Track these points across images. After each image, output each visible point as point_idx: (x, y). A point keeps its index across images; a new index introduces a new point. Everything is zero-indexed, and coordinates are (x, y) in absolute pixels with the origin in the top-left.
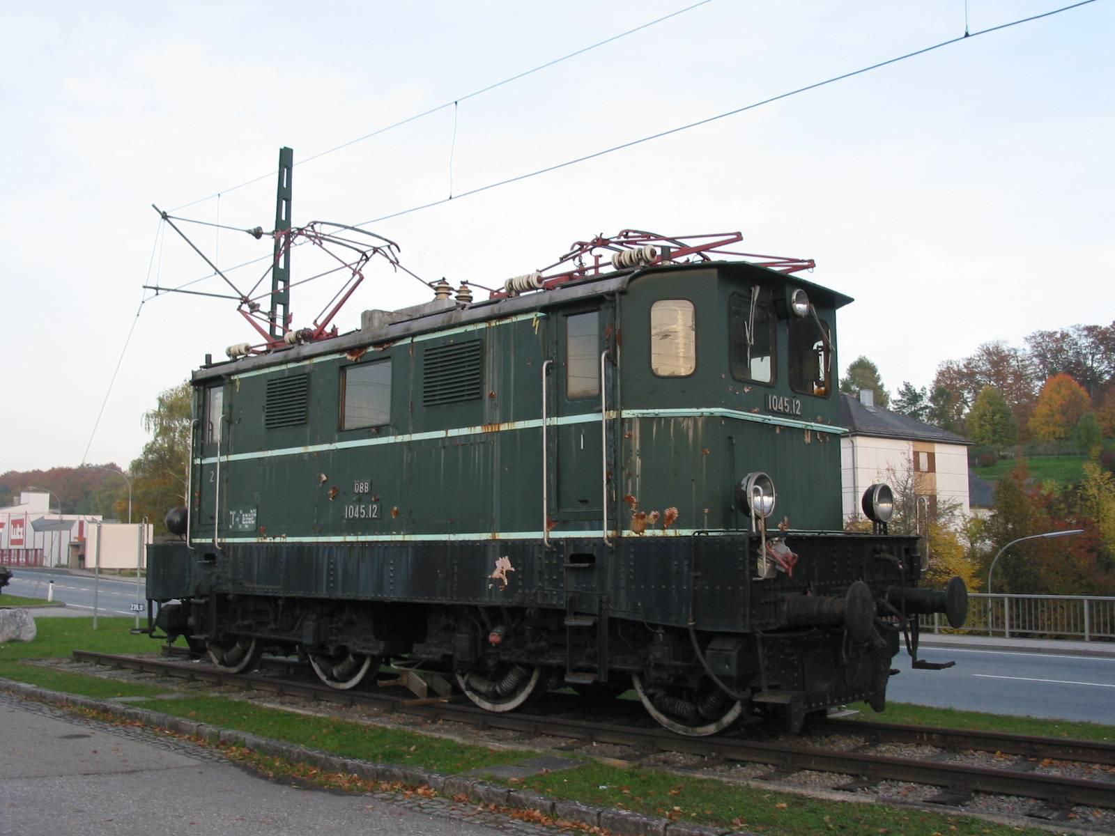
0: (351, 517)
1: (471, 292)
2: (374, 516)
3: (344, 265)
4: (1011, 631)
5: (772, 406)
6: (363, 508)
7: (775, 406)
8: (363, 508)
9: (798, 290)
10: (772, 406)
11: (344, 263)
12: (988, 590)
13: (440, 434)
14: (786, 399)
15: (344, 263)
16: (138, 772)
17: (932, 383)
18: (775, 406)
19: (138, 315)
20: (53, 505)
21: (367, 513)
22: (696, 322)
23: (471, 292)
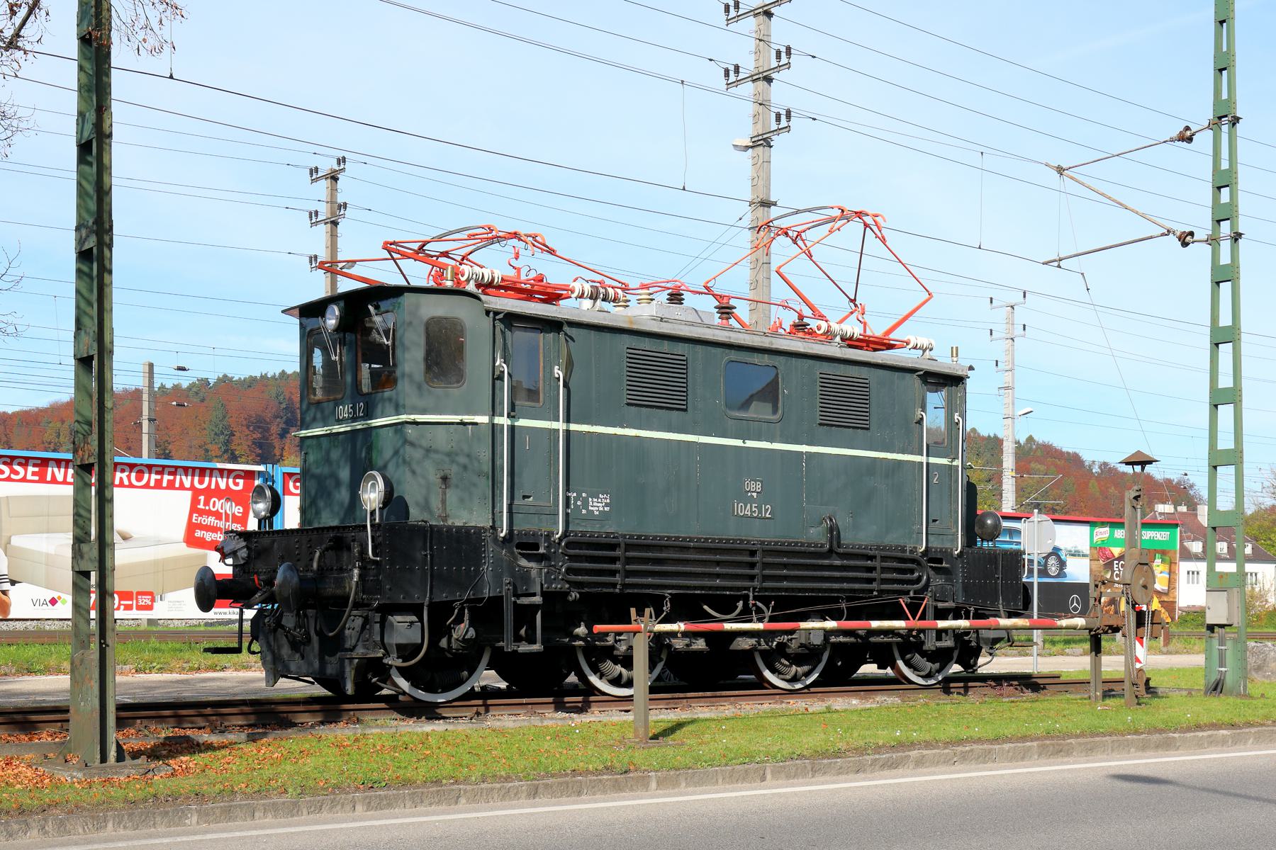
0: (742, 514)
1: (683, 295)
2: (767, 516)
3: (868, 229)
4: (766, 620)
5: (737, 512)
6: (755, 507)
7: (741, 512)
8: (755, 507)
9: (372, 482)
10: (737, 512)
11: (865, 230)
12: (1022, 467)
13: (751, 444)
14: (754, 505)
15: (865, 230)
16: (1199, 789)
17: (1050, 443)
18: (741, 512)
19: (1088, 289)
20: (879, 668)
21: (760, 512)
22: (99, 477)
23: (683, 295)
